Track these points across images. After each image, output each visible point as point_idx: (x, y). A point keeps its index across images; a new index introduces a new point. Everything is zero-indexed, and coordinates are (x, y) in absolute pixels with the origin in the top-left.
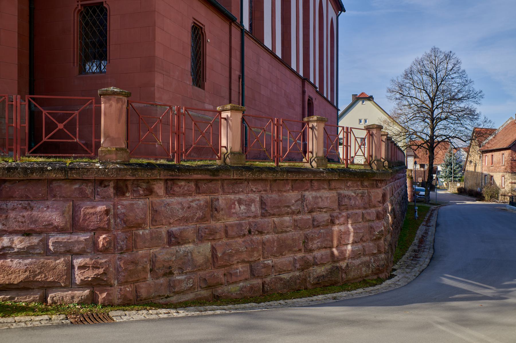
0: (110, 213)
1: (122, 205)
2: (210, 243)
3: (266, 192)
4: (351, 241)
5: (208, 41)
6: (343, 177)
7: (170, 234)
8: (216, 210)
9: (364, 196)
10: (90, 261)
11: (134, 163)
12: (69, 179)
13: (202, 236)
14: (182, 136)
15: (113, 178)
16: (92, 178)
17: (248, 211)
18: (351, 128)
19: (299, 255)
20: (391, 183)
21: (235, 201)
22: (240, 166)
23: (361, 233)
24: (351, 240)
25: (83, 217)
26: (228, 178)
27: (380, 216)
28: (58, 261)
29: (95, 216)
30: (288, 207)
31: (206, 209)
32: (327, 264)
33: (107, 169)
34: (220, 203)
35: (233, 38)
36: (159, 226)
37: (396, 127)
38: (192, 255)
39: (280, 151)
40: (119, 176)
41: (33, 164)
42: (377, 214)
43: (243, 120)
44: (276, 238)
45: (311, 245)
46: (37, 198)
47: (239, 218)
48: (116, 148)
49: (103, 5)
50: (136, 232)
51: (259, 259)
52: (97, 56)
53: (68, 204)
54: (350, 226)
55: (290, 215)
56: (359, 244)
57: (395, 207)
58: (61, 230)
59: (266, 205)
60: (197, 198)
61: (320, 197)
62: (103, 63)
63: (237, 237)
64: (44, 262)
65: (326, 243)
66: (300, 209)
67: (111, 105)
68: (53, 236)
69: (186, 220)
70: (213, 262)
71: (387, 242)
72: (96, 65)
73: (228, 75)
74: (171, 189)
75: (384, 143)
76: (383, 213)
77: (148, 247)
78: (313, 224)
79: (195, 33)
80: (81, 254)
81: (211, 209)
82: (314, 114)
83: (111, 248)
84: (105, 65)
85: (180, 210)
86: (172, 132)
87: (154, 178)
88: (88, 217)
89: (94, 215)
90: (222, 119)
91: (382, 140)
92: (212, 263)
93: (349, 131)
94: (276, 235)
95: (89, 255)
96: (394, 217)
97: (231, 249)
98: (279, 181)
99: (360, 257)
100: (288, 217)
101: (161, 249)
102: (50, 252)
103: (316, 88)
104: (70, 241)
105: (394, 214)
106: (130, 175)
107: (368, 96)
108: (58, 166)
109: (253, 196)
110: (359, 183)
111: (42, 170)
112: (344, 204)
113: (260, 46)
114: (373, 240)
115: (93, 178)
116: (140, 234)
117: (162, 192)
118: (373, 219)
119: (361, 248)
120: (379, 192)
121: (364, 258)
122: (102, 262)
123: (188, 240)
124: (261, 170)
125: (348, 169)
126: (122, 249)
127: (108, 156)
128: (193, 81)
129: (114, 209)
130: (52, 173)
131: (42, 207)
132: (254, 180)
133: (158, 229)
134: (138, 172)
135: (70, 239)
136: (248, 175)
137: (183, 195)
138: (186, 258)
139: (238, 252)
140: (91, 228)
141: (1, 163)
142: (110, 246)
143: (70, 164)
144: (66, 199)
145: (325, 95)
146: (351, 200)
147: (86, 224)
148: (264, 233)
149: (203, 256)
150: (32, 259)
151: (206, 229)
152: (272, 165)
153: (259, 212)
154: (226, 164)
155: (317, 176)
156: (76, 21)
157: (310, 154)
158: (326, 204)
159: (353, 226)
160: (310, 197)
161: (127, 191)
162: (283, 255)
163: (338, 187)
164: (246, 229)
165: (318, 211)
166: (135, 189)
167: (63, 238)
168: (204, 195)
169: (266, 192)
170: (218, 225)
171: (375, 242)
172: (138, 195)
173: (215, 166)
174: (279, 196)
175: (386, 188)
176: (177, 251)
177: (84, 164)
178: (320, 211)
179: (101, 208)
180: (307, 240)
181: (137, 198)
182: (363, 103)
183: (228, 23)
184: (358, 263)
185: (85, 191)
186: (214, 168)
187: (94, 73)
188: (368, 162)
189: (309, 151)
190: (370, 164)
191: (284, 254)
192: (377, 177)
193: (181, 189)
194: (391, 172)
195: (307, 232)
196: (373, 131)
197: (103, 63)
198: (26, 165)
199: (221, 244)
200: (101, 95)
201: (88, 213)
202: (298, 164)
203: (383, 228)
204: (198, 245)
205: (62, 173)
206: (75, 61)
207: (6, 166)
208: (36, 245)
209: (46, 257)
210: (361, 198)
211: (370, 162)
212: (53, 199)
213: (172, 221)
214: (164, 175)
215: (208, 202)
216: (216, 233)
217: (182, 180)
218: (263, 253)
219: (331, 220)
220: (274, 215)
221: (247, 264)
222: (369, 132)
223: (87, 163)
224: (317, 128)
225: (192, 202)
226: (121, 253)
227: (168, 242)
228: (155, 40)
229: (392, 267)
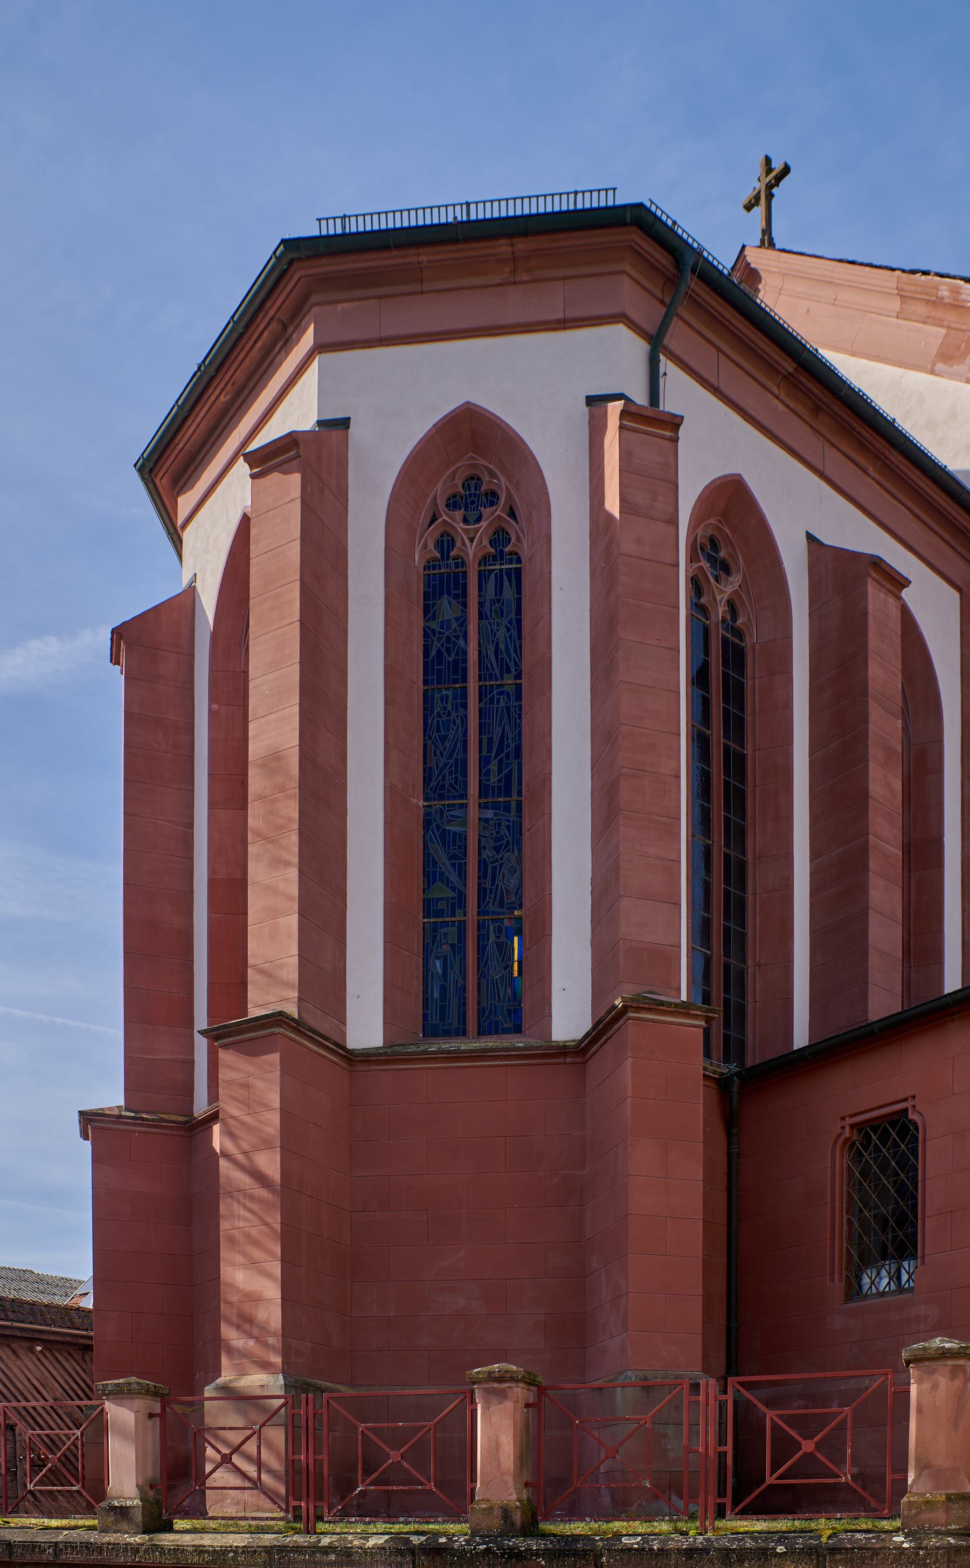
33: (922, 1549)
41: (742, 1539)
49: (907, 1118)
52: (891, 1249)
67: (935, 1387)
72: (889, 1273)
84: (911, 1271)
108: (802, 1544)
111: (763, 1553)
127: (926, 1516)
141: (676, 1564)
143: (829, 1537)
177: (865, 1538)
187: (882, 1294)
198: (728, 1542)
205: (812, 1560)
206: (836, 1271)
207: (683, 1545)
223: (871, 1535)
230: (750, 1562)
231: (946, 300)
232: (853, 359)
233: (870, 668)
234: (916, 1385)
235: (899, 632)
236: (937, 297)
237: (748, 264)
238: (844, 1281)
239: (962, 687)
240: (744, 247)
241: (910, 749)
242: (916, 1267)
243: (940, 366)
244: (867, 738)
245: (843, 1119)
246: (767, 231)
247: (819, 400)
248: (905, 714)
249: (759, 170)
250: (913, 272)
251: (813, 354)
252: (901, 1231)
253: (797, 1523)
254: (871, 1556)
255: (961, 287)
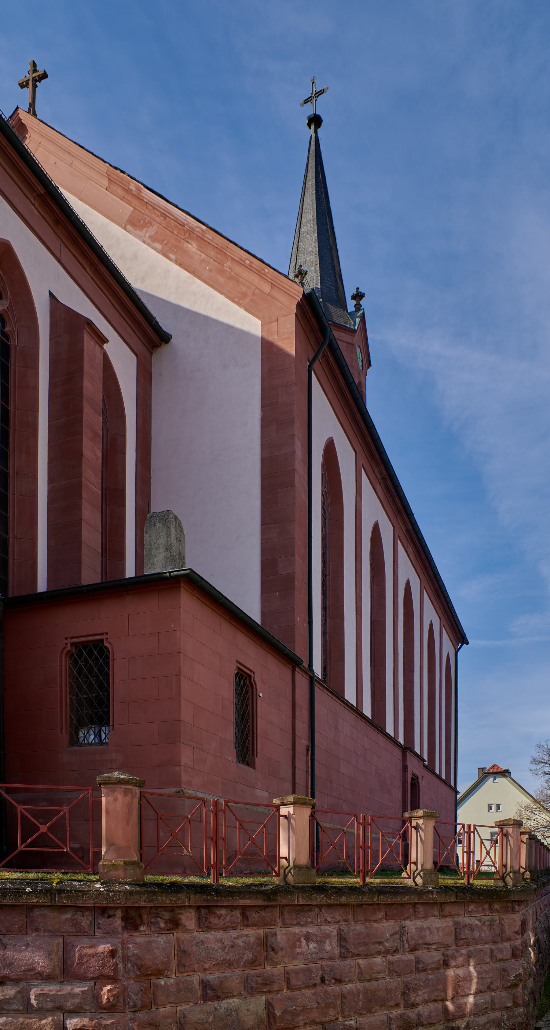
0: (118, 955)
1: (134, 943)
2: (264, 996)
3: (346, 923)
4: (473, 988)
5: (260, 696)
6: (462, 899)
7: (205, 985)
8: (273, 950)
9: (493, 925)
10: (90, 1022)
11: (151, 883)
12: (56, 906)
13: (252, 987)
14: (221, 842)
15: (120, 905)
16: (89, 905)
17: (321, 951)
18: (475, 826)
19: (396, 1012)
20: (534, 903)
21: (301, 936)
22: (307, 887)
23: (488, 978)
24: (474, 988)
25: (78, 960)
26: (290, 904)
27: (515, 954)
28: (44, 1022)
29: (96, 959)
30: (380, 943)
31: (258, 949)
32: (438, 1024)
33: (111, 892)
34: (278, 940)
35: (297, 690)
36: (189, 974)
37: (544, 816)
38: (238, 1015)
39: (368, 862)
40: (129, 902)
41: (5, 883)
42: (513, 950)
43: (312, 816)
44: (361, 989)
45: (414, 998)
46: (12, 932)
47: (307, 961)
48: (124, 861)
49: (103, 644)
50: (156, 981)
51: (337, 1019)
53: (57, 942)
54: (472, 969)
55: (383, 955)
56: (485, 994)
57: (540, 938)
58: (48, 978)
59: (347, 942)
60: (245, 932)
61: (427, 927)
62: (104, 730)
63: (304, 988)
64: (23, 1022)
65: (436, 993)
66: (397, 946)
67: (115, 799)
68: (36, 986)
69: (228, 964)
70: (269, 1024)
71: (527, 991)
72: (94, 733)
73: (289, 745)
74: (206, 921)
75: (525, 845)
76: (521, 948)
77: (173, 1003)
78: (418, 968)
79: (240, 685)
80: (75, 1012)
81: (265, 948)
82: (421, 806)
83: (120, 1005)
84: (107, 733)
85: (220, 950)
86: (207, 837)
87: (181, 905)
88: (85, 960)
89: (93, 957)
90: (281, 818)
91: (522, 841)
92: (267, 1025)
93: (472, 830)
94: (362, 984)
95: (88, 1013)
96: (539, 951)
97: (296, 1005)
98: (366, 906)
99: (486, 1013)
100: (380, 958)
101: (192, 1006)
102: (31, 1009)
103: (424, 761)
104: (60, 993)
105: (539, 948)
106: (145, 901)
107: (502, 771)
109: (327, 929)
110: (486, 906)
111: (18, 892)
112: (463, 937)
113: (338, 701)
114: (506, 988)
115: (91, 904)
116: (161, 985)
117: (193, 924)
118: (507, 958)
119: (488, 1000)
120: (516, 919)
121: (493, 1014)
122: (108, 1023)
123: (232, 993)
124: (340, 891)
125: (469, 886)
126: (135, 1006)
127: (113, 873)
128: (238, 757)
129: (123, 949)
130: (32, 897)
131: (18, 945)
132: (330, 906)
133: (187, 978)
134: (157, 897)
135: (59, 991)
136: (320, 899)
137: (223, 928)
138: (229, 1018)
139: (305, 1009)
140: (90, 975)
142: (118, 1001)
143: (58, 883)
144: (53, 933)
145: (437, 771)
146: (473, 932)
147: (82, 970)
148: (344, 981)
149: (253, 1016)
150: (7, 1017)
151: (258, 976)
152: (356, 883)
153: (336, 952)
154: (287, 883)
155: (423, 898)
156: (63, 667)
157: (413, 865)
158: (437, 937)
159: (477, 969)
160: (413, 928)
161: (142, 923)
162: (371, 1013)
163: (454, 913)
164: (317, 976)
165: (425, 948)
166: (153, 920)
167: (51, 989)
168: (255, 928)
169: (347, 923)
170: (276, 971)
171: (510, 991)
172: (158, 929)
173: (271, 887)
174: (367, 928)
175: (527, 911)
176: (216, 1009)
177: (78, 884)
178: (428, 948)
179: (104, 948)
180: (407, 990)
181: (156, 933)
182: (495, 781)
183: (291, 667)
184: (484, 1022)
185: (80, 923)
186: (269, 890)
187: (90, 744)
188: (500, 875)
189: (412, 861)
190: (503, 878)
191: (373, 1010)
192: (514, 897)
193: (221, 920)
194: (535, 889)
195: (408, 978)
196: (508, 829)
197: (104, 730)
199: (280, 997)
200: (100, 784)
201: (86, 955)
202: (395, 881)
203: (521, 970)
204: (246, 1000)
205: (47, 897)
206: (64, 727)
208: (12, 999)
209: (26, 1015)
210: (489, 927)
211: (503, 875)
212: (35, 934)
213: (207, 966)
214: (195, 899)
215: (260, 938)
216: (273, 982)
217: (222, 906)
218: (343, 1010)
219: (444, 961)
220: (358, 955)
221: (319, 1026)
222: (502, 830)
223: (82, 883)
224: (423, 827)
225: (237, 938)
226: (135, 1011)
227: (203, 996)
228: (180, 696)
229: (535, 1025)
230: (10, 897)
231: (133, 192)
232: (80, 202)
233: (84, 381)
234: (105, 797)
235: (102, 367)
236: (129, 188)
237: (20, 120)
238: (68, 734)
239: (137, 409)
240: (17, 108)
241: (107, 436)
242: (110, 731)
243: (129, 227)
244: (82, 421)
245: (66, 639)
246: (32, 105)
247: (59, 216)
248: (104, 413)
249: (29, 67)
250: (116, 168)
251: (56, 189)
252: (100, 709)
253: (40, 875)
254: (82, 895)
255: (142, 189)
